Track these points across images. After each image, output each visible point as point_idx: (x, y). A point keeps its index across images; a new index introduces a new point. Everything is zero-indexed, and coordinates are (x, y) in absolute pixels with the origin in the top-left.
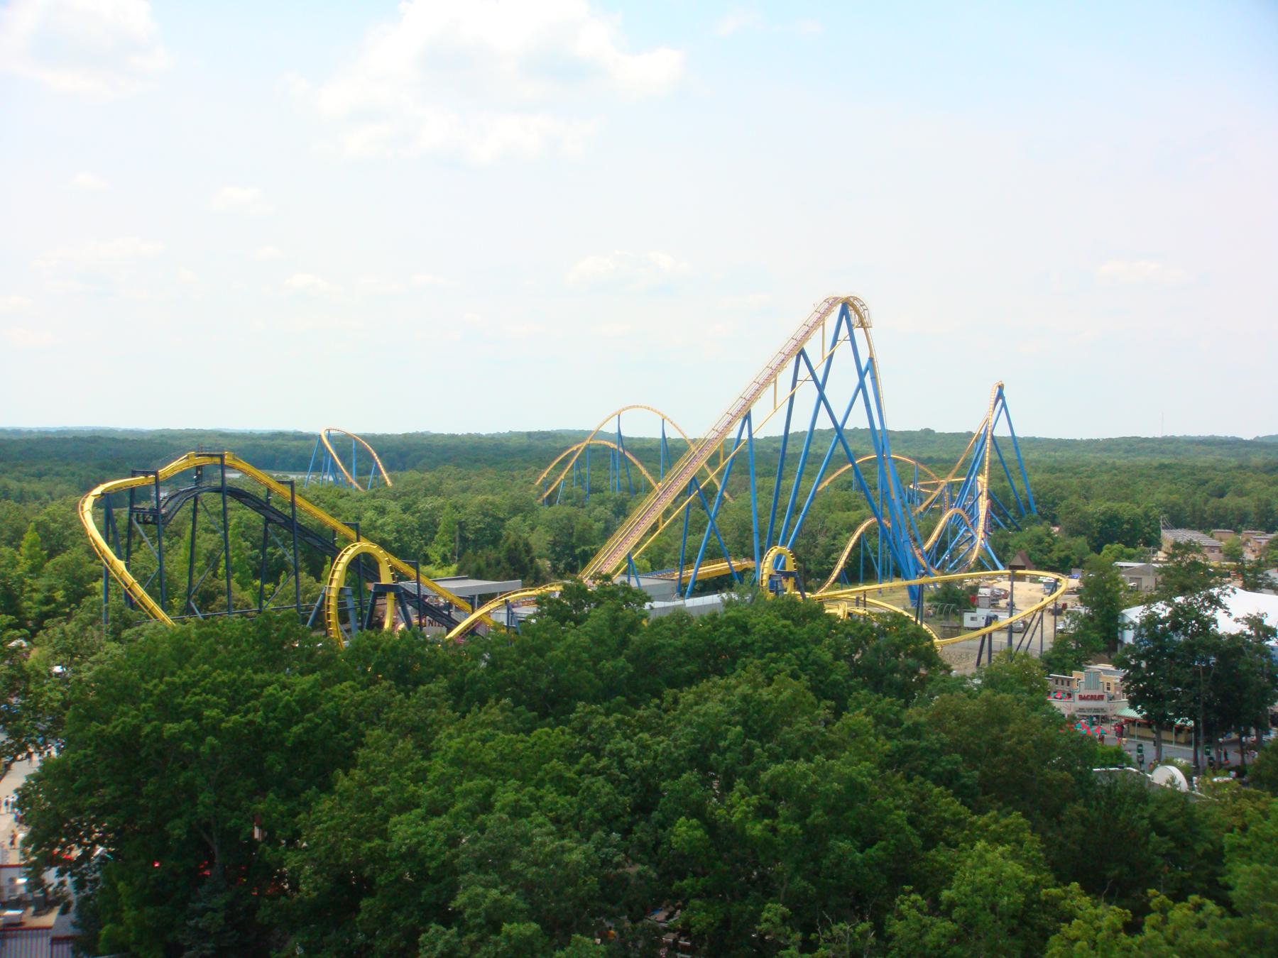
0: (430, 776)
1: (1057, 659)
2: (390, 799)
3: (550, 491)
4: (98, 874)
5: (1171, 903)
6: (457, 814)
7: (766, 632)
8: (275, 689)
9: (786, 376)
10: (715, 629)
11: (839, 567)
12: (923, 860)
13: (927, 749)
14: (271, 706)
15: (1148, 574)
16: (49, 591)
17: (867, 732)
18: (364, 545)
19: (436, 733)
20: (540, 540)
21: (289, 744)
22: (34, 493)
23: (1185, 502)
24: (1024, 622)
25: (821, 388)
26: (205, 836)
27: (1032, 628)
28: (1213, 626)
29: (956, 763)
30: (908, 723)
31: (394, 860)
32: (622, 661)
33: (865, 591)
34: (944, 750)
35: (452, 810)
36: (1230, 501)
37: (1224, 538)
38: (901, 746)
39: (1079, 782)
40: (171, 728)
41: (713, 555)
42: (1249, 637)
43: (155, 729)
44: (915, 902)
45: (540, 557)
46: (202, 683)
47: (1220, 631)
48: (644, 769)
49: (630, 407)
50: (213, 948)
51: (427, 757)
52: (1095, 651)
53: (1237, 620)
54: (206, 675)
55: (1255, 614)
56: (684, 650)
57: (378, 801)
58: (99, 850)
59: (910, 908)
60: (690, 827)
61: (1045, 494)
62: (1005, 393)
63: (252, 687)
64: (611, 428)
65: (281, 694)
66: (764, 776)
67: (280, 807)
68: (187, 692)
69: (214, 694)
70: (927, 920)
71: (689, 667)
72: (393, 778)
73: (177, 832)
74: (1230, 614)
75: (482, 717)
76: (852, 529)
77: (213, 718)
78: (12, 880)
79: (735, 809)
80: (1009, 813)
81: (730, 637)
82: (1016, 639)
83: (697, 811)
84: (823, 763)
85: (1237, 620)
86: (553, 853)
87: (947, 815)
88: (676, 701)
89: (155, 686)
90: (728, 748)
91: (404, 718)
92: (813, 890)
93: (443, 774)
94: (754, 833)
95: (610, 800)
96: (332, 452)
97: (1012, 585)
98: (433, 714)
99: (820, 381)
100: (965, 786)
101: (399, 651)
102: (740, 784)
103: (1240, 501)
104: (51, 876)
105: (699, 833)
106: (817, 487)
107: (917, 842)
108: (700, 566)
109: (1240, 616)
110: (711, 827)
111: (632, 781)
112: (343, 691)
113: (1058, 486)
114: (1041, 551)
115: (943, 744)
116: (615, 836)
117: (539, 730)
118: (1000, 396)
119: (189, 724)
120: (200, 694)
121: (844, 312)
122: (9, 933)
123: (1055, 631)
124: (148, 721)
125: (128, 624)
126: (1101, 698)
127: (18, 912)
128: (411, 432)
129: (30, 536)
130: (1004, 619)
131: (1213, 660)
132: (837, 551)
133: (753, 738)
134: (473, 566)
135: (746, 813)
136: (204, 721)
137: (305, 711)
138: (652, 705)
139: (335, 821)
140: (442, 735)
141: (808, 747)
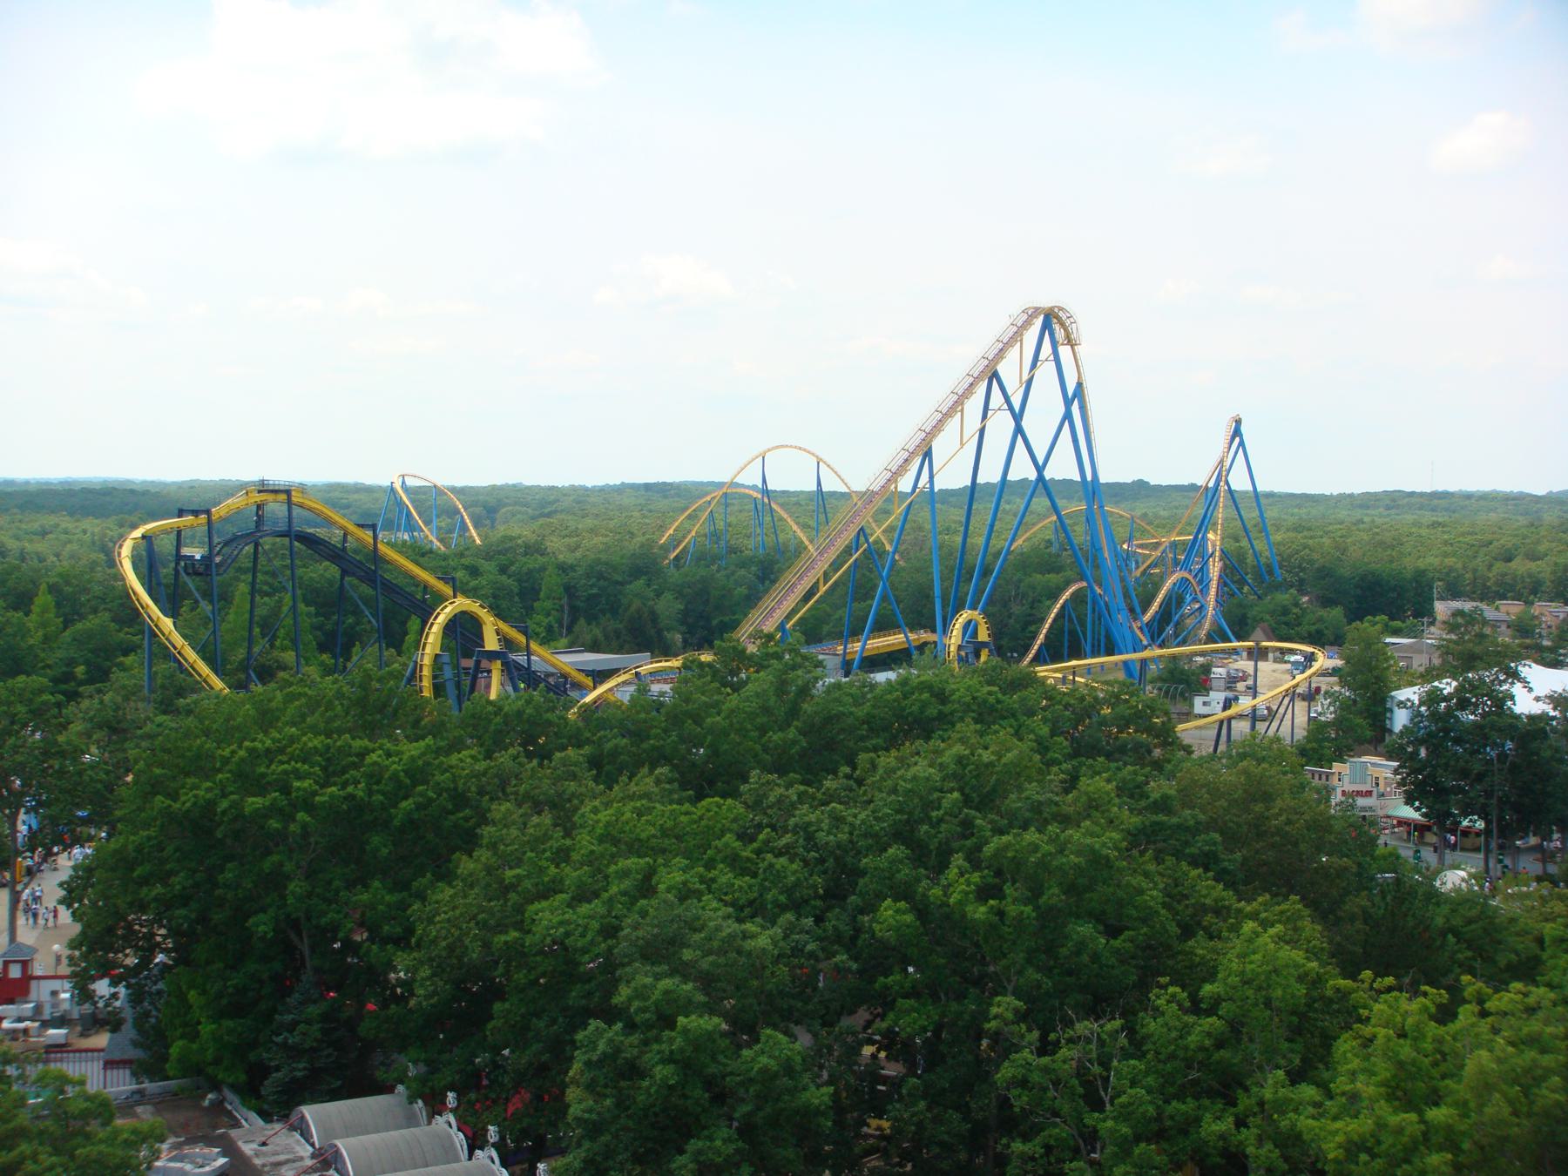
0: (575, 856)
1: (1313, 749)
2: (527, 884)
3: (677, 551)
4: (161, 986)
5: (1490, 991)
6: (611, 899)
7: (968, 699)
8: (380, 756)
9: (974, 404)
10: (905, 697)
11: (1039, 642)
12: (1179, 953)
13: (1179, 826)
14: (375, 777)
15: (1421, 652)
16: (68, 665)
17: (1109, 802)
18: (462, 603)
19: (576, 809)
20: (668, 607)
21: (396, 822)
22: (37, 554)
23: (1464, 567)
24: (1268, 708)
25: (1018, 418)
26: (293, 936)
27: (1279, 716)
28: (1509, 703)
29: (1215, 844)
30: (1155, 796)
31: (535, 955)
32: (792, 733)
33: (1074, 667)
34: (1195, 830)
35: (605, 895)
36: (1520, 566)
37: (1510, 609)
38: (1147, 823)
39: (1359, 875)
40: (254, 802)
41: (882, 626)
42: (1554, 718)
43: (234, 805)
44: (1174, 996)
45: (668, 630)
46: (289, 750)
47: (1518, 709)
48: (839, 845)
49: (777, 447)
50: (305, 1069)
51: (568, 834)
52: (1361, 741)
53: (1537, 699)
54: (292, 740)
55: (1560, 691)
56: (868, 720)
57: (512, 887)
58: (160, 958)
59: (1169, 1002)
60: (898, 911)
61: (1291, 556)
62: (1243, 429)
63: (350, 755)
64: (751, 478)
65: (387, 763)
66: (988, 850)
67: (388, 898)
68: (271, 762)
69: (304, 762)
70: (1191, 1019)
71: (874, 742)
72: (530, 858)
73: (262, 928)
74: (1530, 690)
75: (633, 788)
76: (1054, 596)
77: (305, 790)
78: (54, 993)
79: (951, 889)
80: (1286, 898)
81: (924, 705)
82: (1261, 727)
83: (904, 893)
84: (1057, 835)
85: (1537, 699)
86: (732, 936)
87: (1208, 901)
88: (874, 767)
89: (233, 752)
90: (941, 820)
91: (537, 791)
92: (1048, 984)
93: (592, 852)
94: (977, 916)
95: (798, 879)
96: (408, 503)
97: (1256, 665)
98: (572, 786)
99: (1017, 409)
100: (1225, 871)
101: (525, 716)
102: (958, 860)
103: (1533, 566)
104: (102, 987)
105: (909, 918)
106: (1011, 545)
107: (1174, 929)
108: (868, 638)
109: (1542, 694)
110: (922, 911)
111: (822, 861)
112: (461, 760)
113: (1305, 547)
114: (1286, 624)
115: (1197, 823)
116: (808, 922)
117: (710, 800)
118: (1237, 432)
119: (275, 799)
120: (288, 762)
121: (1047, 326)
122: (53, 1055)
123: (1310, 718)
124: (224, 796)
125: (181, 693)
126: (1369, 794)
127: (63, 1031)
128: (499, 483)
129: (43, 599)
130: (1245, 703)
131: (1509, 745)
132: (1034, 622)
133: (971, 808)
134: (588, 638)
135: (967, 893)
136: (294, 794)
137: (415, 785)
138: (841, 774)
139: (458, 912)
140: (586, 809)
141: (1038, 816)
